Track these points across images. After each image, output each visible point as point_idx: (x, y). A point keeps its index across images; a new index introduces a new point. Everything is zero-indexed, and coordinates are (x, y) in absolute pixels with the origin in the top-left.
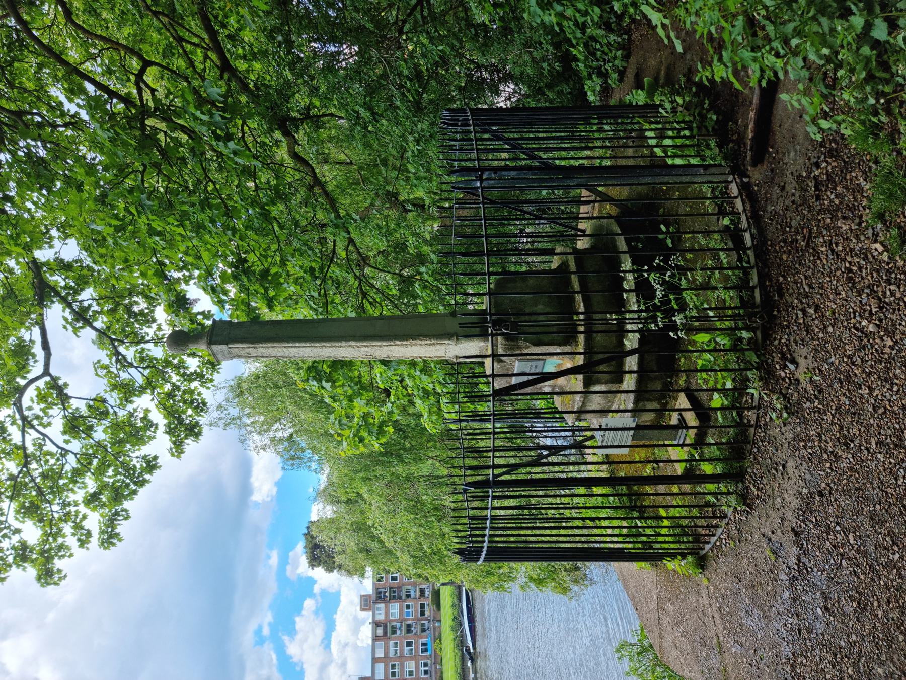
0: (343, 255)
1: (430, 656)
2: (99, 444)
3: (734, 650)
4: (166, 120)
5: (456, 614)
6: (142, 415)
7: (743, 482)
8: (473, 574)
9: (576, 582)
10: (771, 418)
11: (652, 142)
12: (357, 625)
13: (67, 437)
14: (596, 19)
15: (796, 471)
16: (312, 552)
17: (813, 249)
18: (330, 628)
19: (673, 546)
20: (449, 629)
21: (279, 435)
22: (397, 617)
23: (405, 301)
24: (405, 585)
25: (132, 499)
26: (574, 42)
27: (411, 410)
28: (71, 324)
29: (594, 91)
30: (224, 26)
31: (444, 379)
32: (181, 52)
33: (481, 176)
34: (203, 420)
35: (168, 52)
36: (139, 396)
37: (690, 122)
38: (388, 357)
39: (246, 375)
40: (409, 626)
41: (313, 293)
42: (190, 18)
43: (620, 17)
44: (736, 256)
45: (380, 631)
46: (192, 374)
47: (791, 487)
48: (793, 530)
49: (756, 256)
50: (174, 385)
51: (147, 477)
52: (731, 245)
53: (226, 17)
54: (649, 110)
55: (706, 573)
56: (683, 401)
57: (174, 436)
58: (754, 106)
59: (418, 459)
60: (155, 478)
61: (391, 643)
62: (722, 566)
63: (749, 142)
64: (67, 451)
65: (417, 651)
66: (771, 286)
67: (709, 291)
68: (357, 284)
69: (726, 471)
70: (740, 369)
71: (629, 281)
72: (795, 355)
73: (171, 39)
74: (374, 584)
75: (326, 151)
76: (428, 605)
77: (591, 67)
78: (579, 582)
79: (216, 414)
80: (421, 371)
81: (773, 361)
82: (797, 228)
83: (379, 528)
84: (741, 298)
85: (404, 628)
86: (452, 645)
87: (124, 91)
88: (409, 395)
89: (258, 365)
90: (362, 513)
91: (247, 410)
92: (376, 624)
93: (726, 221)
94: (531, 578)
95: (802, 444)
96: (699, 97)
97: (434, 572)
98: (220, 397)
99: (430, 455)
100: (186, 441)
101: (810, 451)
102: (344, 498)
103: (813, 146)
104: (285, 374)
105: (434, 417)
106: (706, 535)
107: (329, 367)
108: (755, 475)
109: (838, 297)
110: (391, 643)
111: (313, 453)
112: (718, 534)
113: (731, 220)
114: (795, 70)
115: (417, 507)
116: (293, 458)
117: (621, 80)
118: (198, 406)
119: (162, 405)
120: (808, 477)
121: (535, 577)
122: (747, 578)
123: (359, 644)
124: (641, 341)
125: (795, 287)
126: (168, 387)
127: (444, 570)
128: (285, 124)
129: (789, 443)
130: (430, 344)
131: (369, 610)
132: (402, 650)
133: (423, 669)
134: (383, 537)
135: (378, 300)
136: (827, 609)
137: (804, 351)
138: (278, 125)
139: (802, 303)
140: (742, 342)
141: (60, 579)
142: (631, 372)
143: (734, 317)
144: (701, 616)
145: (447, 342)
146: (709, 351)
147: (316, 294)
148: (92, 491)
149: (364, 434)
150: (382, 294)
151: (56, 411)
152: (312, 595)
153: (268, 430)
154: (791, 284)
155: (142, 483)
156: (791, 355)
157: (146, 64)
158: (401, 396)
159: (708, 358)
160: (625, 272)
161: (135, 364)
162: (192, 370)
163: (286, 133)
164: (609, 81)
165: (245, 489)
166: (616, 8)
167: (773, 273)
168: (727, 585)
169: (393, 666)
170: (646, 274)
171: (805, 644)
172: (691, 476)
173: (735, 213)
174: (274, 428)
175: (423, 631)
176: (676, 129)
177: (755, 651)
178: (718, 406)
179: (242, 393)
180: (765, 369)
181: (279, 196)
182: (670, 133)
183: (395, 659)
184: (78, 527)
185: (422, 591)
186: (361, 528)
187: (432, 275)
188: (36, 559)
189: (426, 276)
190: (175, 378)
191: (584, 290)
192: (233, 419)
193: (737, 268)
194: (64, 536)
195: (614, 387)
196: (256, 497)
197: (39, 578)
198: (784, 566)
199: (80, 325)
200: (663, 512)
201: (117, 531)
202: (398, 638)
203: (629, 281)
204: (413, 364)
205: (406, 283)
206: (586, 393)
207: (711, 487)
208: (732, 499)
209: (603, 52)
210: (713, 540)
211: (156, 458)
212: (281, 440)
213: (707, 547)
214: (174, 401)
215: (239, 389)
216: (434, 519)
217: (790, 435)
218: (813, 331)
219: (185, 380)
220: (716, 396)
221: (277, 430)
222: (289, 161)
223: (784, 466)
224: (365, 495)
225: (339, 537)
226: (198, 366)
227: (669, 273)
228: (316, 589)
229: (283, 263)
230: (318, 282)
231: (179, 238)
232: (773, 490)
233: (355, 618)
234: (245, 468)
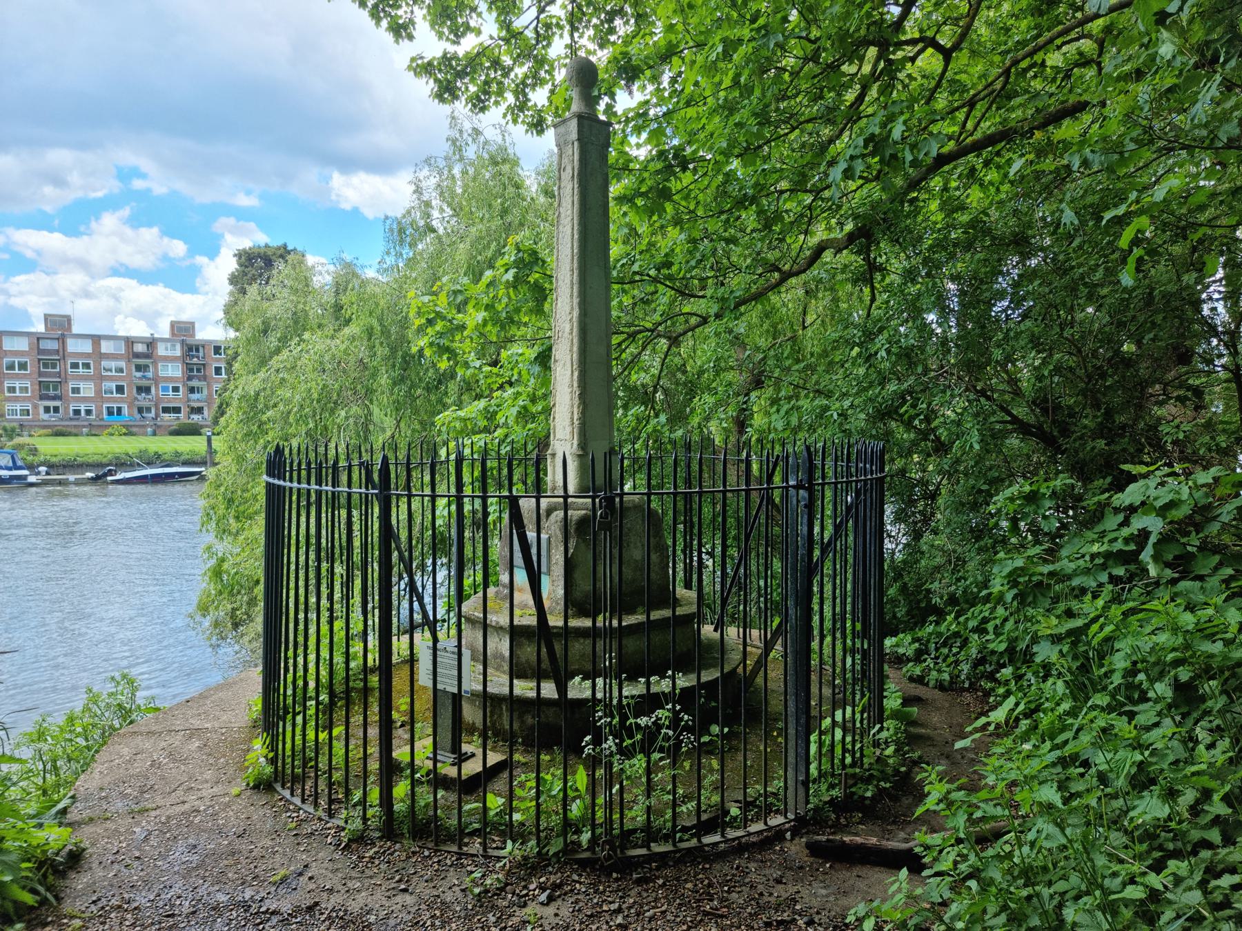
0: (686, 309)
1: (102, 419)
3: (137, 830)
4: (874, 76)
5: (166, 457)
6: (472, 24)
7: (380, 838)
8: (229, 480)
9: (216, 624)
10: (472, 872)
11: (839, 715)
12: (149, 317)
14: (991, 646)
15: (399, 906)
16: (259, 256)
17: (701, 920)
18: (144, 277)
20: (143, 447)
21: (436, 214)
22: (161, 374)
24: (209, 386)
26: (962, 619)
29: (897, 645)
30: (987, 163)
32: (956, 105)
33: (803, 487)
34: (461, 107)
35: (957, 87)
36: (497, 20)
37: (862, 764)
38: (556, 361)
39: (520, 172)
42: (998, 120)
43: (991, 677)
44: (689, 824)
45: (140, 348)
46: (525, 95)
47: (378, 899)
48: (317, 904)
49: (689, 850)
50: (511, 69)
51: (384, 23)
52: (704, 817)
53: (998, 167)
54: (877, 714)
55: (249, 793)
56: (494, 758)
57: (439, 64)
58: (884, 842)
61: (123, 364)
62: (260, 812)
63: (838, 838)
65: (109, 400)
66: (651, 869)
67: (645, 790)
68: (649, 325)
69: (396, 815)
70: (538, 831)
71: (662, 686)
72: (559, 902)
73: (972, 92)
74: (211, 342)
75: (820, 295)
76: (178, 418)
77: (928, 641)
78: (215, 627)
79: (467, 126)
80: (525, 407)
81: (551, 873)
82: (727, 900)
83: (299, 348)
84: (634, 831)
85: (144, 383)
86: (117, 450)
87: (908, 25)
89: (534, 189)
90: (320, 326)
91: (471, 171)
92: (151, 343)
93: (735, 811)
94: (223, 560)
95: (438, 913)
96: (894, 776)
97: (233, 425)
98: (491, 134)
99: (402, 425)
100: (431, 81)
101: (429, 923)
102: (344, 300)
103: (835, 917)
104: (522, 224)
106: (303, 790)
107: (536, 281)
108: (392, 854)
110: (123, 364)
112: (305, 807)
113: (735, 818)
114: (936, 889)
115: (328, 403)
116: (402, 231)
117: (911, 679)
119: (483, 52)
120: (392, 922)
121: (225, 566)
122: (243, 845)
123: (119, 318)
125: (650, 899)
126: (507, 60)
127: (235, 439)
128: (863, 238)
129: (438, 896)
130: (572, 419)
131: (173, 334)
132: (111, 379)
133: (83, 409)
134: (285, 354)
135: (624, 355)
137: (565, 912)
138: (864, 226)
139: (629, 908)
140: (574, 833)
143: (609, 821)
144: (184, 787)
145: (576, 442)
146: (565, 789)
147: (636, 268)
149: (439, 326)
150: (632, 361)
152: (192, 252)
154: (654, 895)
155: (375, 15)
156: (559, 896)
157: (947, 54)
158: (489, 381)
159: (552, 788)
160: (673, 679)
161: (542, 16)
162: (531, 95)
163: (851, 238)
164: (911, 664)
165: (348, 164)
166: (1003, 671)
167: (668, 872)
168: (232, 819)
169: (87, 366)
170: (670, 706)
171: (153, 924)
172: (390, 770)
173: (746, 822)
175: (140, 410)
176: (854, 746)
177: (138, 858)
178: (488, 804)
179: (496, 163)
180: (539, 863)
181: (768, 221)
182: (849, 739)
183: (98, 368)
185: (199, 410)
186: (299, 324)
187: (655, 430)
189: (653, 422)
190: (520, 71)
191: (650, 626)
192: (460, 150)
193: (674, 826)
196: (337, 179)
198: (263, 894)
200: (338, 730)
202: (129, 374)
203: (662, 686)
205: (646, 397)
207: (374, 795)
208: (357, 824)
209: (948, 656)
210: (297, 801)
211: (411, 37)
213: (287, 793)
214: (488, 68)
215: (501, 160)
216: (311, 425)
217: (449, 897)
218: (593, 923)
219: (517, 85)
220: (501, 801)
221: (442, 210)
222: (813, 241)
223: (405, 890)
226: (535, 105)
227: (671, 733)
228: (202, 260)
229: (677, 222)
230: (653, 273)
231: (717, 79)
232: (371, 877)
233: (158, 314)
234: (381, 165)
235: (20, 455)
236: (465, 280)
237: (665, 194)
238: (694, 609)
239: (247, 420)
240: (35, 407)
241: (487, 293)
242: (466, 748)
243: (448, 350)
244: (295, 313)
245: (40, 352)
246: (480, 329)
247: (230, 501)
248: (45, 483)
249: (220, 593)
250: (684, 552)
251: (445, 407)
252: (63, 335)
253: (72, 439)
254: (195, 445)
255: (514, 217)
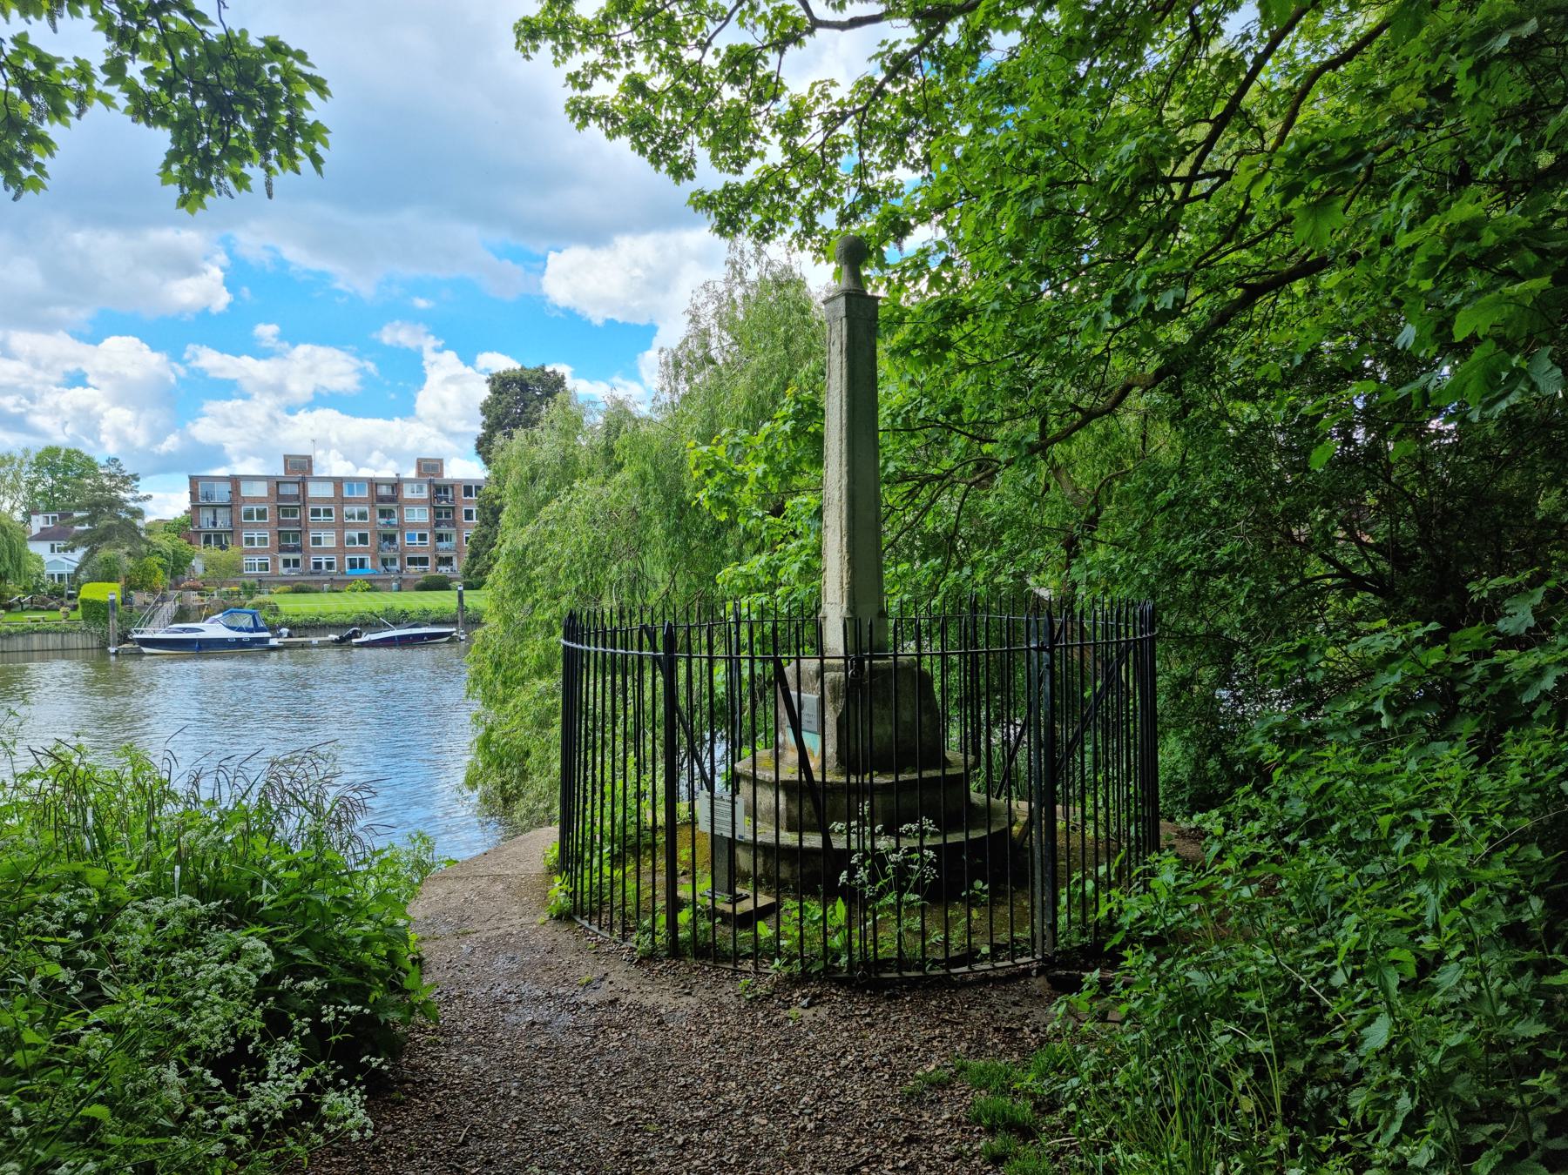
2: (713, 94)
5: (413, 616)
7: (667, 957)
9: (486, 799)
13: (723, 52)
16: (515, 380)
19: (587, 882)
20: (389, 604)
21: (714, 343)
22: (407, 519)
23: (918, 543)
24: (459, 533)
25: (633, 148)
27: (748, 548)
28: (889, 51)
31: (795, 600)
34: (745, 242)
40: (392, 539)
41: (923, 410)
45: (384, 491)
50: (797, 191)
51: (664, 167)
56: (764, 900)
59: (672, 559)
60: (663, 176)
62: (563, 935)
64: (704, 51)
74: (461, 481)
76: (425, 571)
85: (390, 530)
86: (362, 609)
88: (774, 544)
92: (396, 485)
94: (492, 730)
97: (500, 582)
102: (616, 445)
105: (740, 583)
109: (876, 1043)
111: (684, 397)
115: (600, 557)
116: (677, 364)
118: (764, 230)
119: (770, 174)
121: (494, 736)
122: (554, 959)
124: (840, 851)
126: (793, 182)
131: (419, 473)
133: (324, 561)
134: (555, 504)
136: (533, 1023)
141: (525, 49)
142: (801, 840)
143: (864, 952)
148: (649, 85)
151: (762, 32)
153: (721, 325)
155: (655, 160)
163: (1160, 375)
169: (328, 512)
174: (724, 333)
175: (384, 562)
184: (596, 70)
186: (568, 470)
188: (553, 15)
189: (952, 575)
190: (807, 193)
192: (740, 274)
194: (583, 50)
195: (783, 822)
197: (526, 21)
199: (888, 64)
201: (591, 122)
202: (373, 521)
204: (818, 553)
206: (777, 785)
207: (662, 920)
211: (691, 176)
212: (706, 346)
213: (586, 923)
214: (773, 192)
215: (786, 283)
217: (725, 1000)
221: (720, 338)
224: (618, 477)
225: (554, 435)
230: (941, 418)
235: (263, 614)
236: (744, 433)
237: (946, 345)
238: (962, 770)
239: (515, 577)
240: (275, 560)
241: (765, 445)
242: (739, 890)
243: (728, 502)
244: (564, 458)
245: (280, 497)
246: (761, 482)
247: (498, 665)
248: (287, 646)
249: (489, 765)
250: (979, 724)
251: (725, 560)
252: (303, 478)
253: (312, 596)
254: (444, 601)
255: (800, 345)
